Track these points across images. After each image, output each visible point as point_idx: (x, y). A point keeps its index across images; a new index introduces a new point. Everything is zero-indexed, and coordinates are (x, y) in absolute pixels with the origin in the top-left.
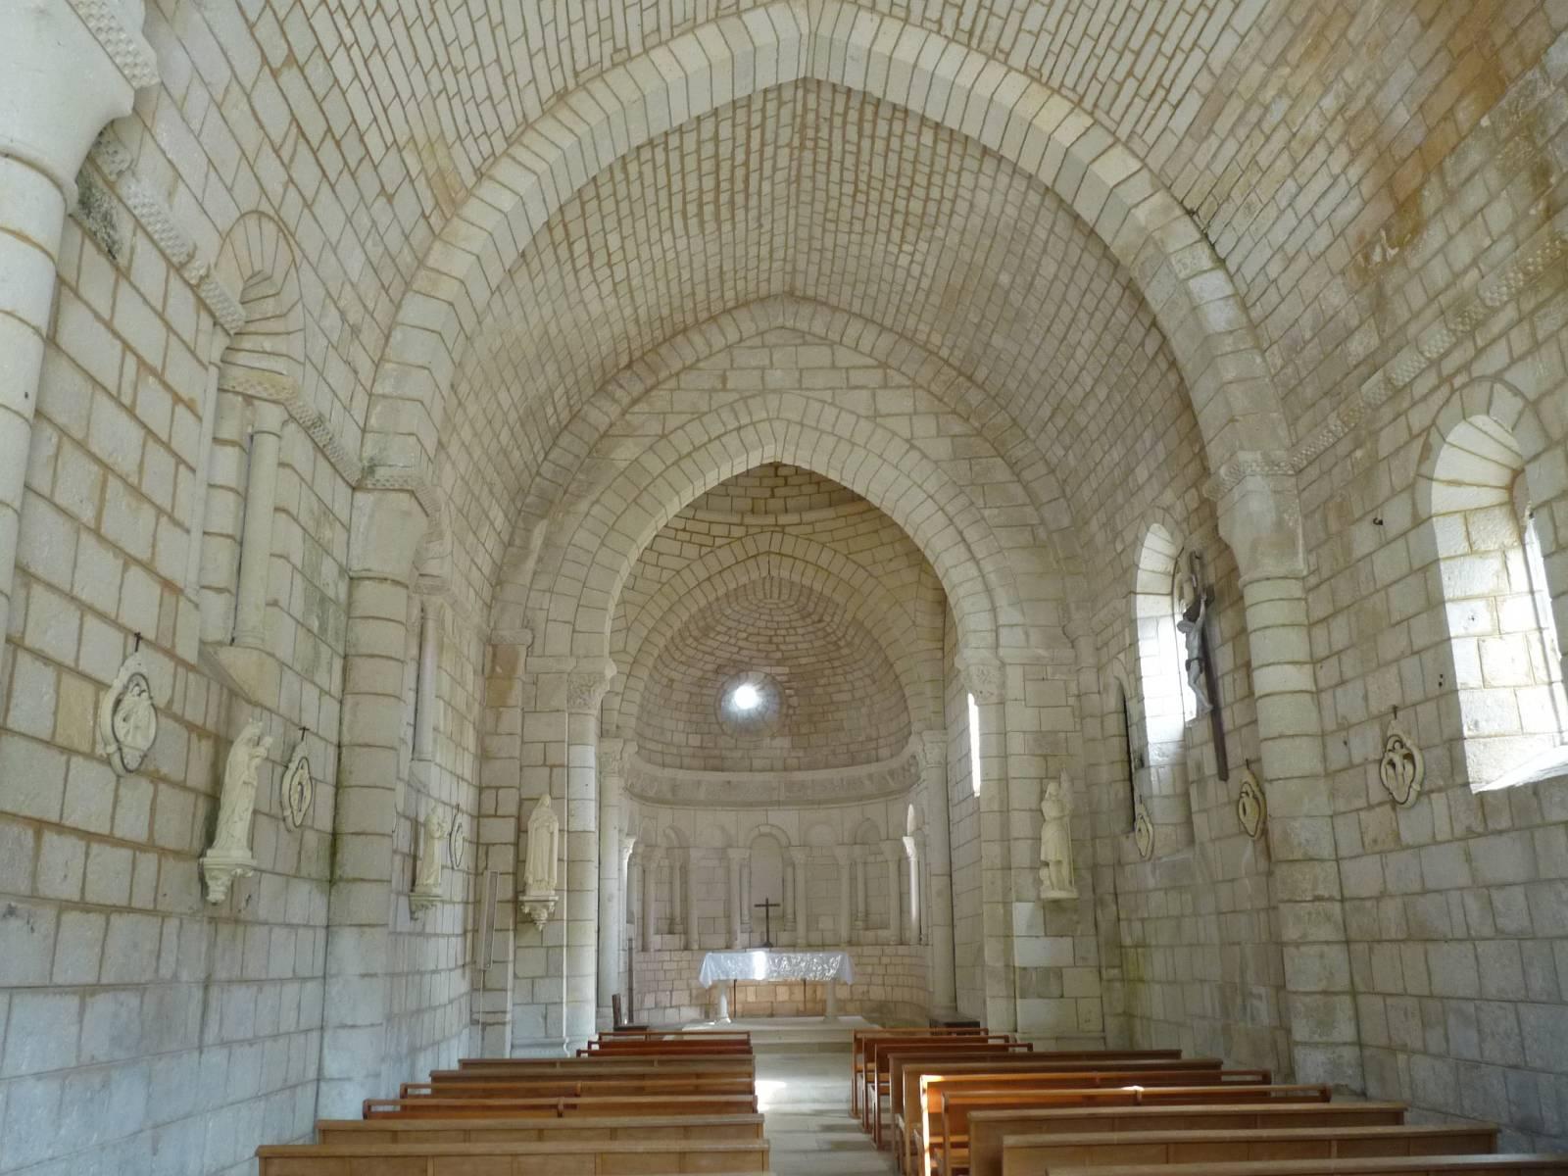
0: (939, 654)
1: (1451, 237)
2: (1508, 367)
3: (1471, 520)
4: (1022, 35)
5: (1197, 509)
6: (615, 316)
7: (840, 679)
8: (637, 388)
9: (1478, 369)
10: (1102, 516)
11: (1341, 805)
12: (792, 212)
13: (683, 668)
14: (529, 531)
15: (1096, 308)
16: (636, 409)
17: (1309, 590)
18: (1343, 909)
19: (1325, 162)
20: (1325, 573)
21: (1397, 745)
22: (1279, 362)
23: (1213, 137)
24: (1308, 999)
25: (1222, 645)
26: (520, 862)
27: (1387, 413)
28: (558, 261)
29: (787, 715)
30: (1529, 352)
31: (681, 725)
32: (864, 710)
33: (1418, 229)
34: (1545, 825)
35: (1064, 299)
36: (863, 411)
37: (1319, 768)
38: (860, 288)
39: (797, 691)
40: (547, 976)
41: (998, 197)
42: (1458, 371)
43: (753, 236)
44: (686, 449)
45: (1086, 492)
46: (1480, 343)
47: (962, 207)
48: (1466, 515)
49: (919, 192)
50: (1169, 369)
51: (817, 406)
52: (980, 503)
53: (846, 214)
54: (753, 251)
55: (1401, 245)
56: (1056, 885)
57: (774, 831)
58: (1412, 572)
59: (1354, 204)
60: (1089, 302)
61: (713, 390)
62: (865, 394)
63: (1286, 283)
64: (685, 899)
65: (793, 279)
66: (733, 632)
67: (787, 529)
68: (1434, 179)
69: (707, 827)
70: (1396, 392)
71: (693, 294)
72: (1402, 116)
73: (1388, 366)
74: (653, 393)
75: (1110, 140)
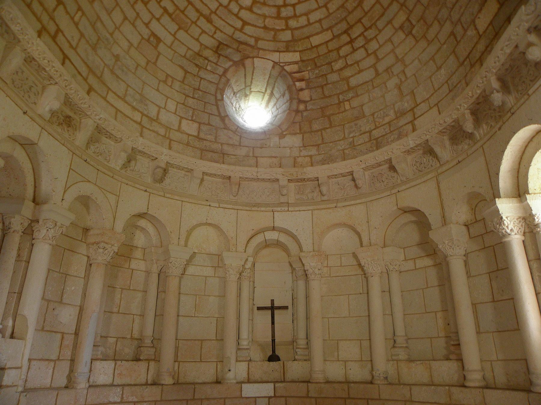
4: (283, 399)
29: (297, 111)
31: (171, 106)
32: (392, 83)
57: (283, 238)
64: (159, 315)
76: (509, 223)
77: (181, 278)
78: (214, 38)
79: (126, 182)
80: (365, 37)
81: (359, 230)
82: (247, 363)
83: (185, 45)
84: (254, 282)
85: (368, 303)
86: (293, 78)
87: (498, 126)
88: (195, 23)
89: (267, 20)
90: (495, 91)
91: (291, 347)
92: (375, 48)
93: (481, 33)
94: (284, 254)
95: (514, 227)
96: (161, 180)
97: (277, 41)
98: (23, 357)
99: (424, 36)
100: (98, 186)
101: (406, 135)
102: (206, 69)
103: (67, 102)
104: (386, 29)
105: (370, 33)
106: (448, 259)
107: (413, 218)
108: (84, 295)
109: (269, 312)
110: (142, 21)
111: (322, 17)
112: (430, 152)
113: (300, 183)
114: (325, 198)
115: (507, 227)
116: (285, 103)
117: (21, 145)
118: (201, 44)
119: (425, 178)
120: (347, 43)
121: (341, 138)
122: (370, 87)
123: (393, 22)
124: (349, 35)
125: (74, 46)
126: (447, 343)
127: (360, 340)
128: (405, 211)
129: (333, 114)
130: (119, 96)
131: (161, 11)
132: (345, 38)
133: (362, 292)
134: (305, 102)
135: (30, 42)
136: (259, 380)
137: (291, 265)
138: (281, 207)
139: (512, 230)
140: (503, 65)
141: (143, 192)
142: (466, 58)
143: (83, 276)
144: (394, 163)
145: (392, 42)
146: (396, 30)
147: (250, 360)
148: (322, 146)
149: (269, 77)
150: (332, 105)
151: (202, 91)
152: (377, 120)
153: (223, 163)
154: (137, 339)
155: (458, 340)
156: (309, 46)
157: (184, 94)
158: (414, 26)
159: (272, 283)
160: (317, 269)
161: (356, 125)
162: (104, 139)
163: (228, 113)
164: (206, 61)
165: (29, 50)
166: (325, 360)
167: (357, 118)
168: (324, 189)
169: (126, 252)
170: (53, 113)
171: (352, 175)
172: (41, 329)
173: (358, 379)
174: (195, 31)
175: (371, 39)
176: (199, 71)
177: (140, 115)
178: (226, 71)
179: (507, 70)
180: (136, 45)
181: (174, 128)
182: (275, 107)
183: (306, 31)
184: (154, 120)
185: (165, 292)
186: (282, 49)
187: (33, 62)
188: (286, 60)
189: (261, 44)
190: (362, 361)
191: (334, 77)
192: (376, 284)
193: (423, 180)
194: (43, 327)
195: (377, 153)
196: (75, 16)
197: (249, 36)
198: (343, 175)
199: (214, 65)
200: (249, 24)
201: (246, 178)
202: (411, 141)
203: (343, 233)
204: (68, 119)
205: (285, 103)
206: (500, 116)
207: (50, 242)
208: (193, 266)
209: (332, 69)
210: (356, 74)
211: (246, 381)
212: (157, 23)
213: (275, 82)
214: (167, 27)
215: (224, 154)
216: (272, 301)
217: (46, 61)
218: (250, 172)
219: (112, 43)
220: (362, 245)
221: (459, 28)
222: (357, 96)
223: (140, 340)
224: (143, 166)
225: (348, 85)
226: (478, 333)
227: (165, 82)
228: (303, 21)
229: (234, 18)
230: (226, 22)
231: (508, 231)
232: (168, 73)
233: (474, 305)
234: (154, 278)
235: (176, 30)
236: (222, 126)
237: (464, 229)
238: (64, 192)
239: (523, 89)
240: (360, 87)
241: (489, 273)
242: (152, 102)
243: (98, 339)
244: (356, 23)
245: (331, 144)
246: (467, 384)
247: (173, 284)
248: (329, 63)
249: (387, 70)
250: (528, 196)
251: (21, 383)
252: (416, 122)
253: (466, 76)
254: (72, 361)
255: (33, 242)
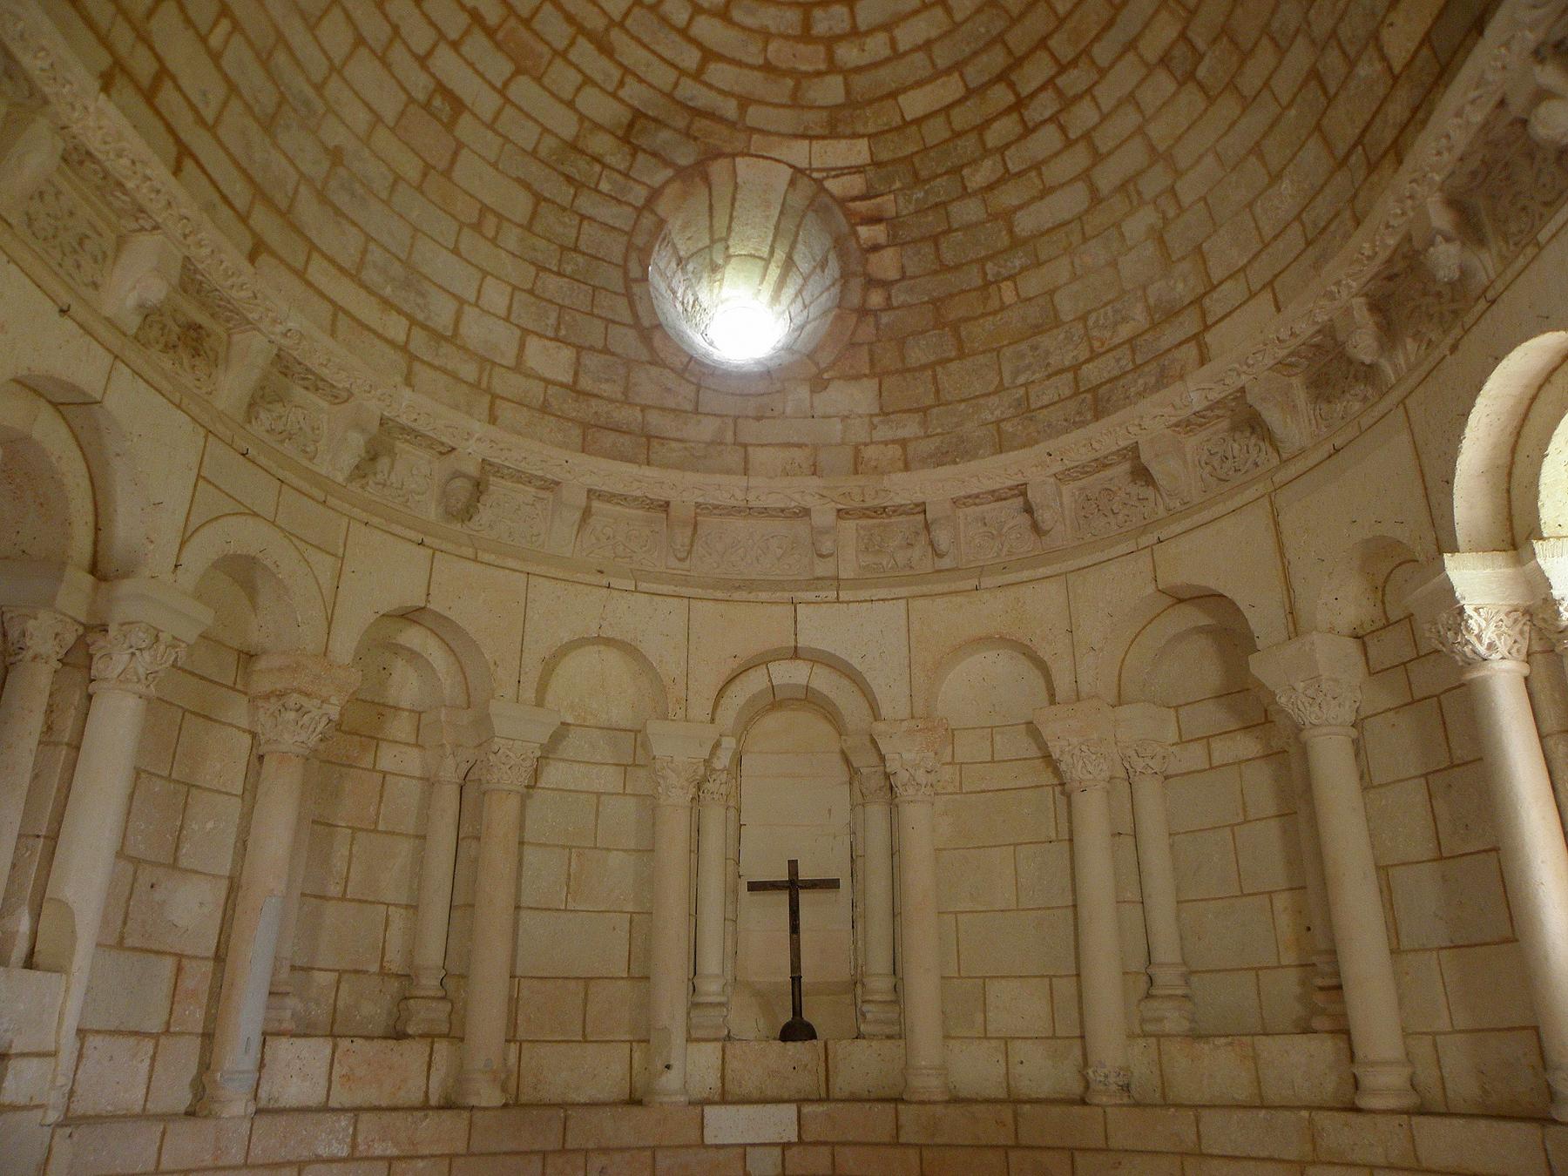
4: (825, 1150)
29: (863, 312)
31: (496, 297)
32: (1139, 224)
57: (823, 681)
64: (462, 907)
76: (1484, 624)
77: (524, 799)
78: (621, 101)
79: (365, 516)
80: (1060, 93)
81: (1045, 653)
82: (719, 1045)
83: (536, 121)
84: (739, 811)
85: (1073, 869)
86: (848, 214)
87: (1449, 341)
88: (563, 54)
89: (773, 46)
90: (1439, 238)
91: (848, 998)
92: (1090, 124)
93: (1397, 70)
94: (826, 727)
95: (1499, 636)
96: (467, 513)
97: (803, 107)
98: (60, 1024)
99: (1231, 85)
100: (282, 530)
101: (1182, 377)
102: (597, 190)
103: (190, 281)
104: (1118, 67)
105: (1074, 81)
106: (1305, 735)
107: (1204, 620)
108: (242, 847)
109: (784, 897)
110: (410, 50)
111: (934, 33)
112: (1252, 424)
113: (871, 522)
114: (946, 563)
115: (1479, 637)
116: (828, 289)
117: (56, 405)
118: (582, 118)
119: (1239, 500)
120: (1008, 110)
121: (992, 388)
122: (1076, 238)
123: (1142, 45)
124: (1012, 86)
125: (210, 120)
126: (1303, 983)
127: (1050, 977)
128: (1180, 598)
129: (966, 320)
130: (341, 269)
131: (464, 19)
132: (1001, 96)
133: (1053, 836)
134: (885, 284)
135: (78, 105)
136: (756, 1095)
137: (847, 761)
138: (817, 589)
139: (1491, 646)
140: (1461, 159)
141: (415, 548)
142: (1355, 146)
143: (240, 792)
144: (1145, 457)
145: (1138, 105)
146: (1150, 69)
147: (729, 1037)
148: (935, 410)
149: (781, 213)
150: (963, 291)
151: (584, 254)
152: (1095, 333)
153: (648, 464)
154: (398, 976)
155: (1337, 974)
156: (897, 121)
157: (533, 263)
158: (1202, 57)
159: (794, 814)
160: (922, 770)
161: (1034, 348)
162: (298, 392)
163: (662, 318)
164: (597, 168)
165: (75, 129)
166: (947, 1037)
167: (1038, 330)
168: (942, 537)
169: (364, 722)
170: (148, 314)
171: (1024, 494)
172: (119, 941)
173: (1044, 1090)
174: (566, 80)
175: (1078, 98)
176: (575, 195)
177: (405, 322)
178: (655, 194)
179: (1474, 174)
180: (390, 118)
181: (504, 362)
182: (799, 300)
183: (887, 77)
184: (446, 339)
185: (478, 839)
186: (818, 131)
187: (87, 163)
188: (831, 163)
189: (755, 116)
190: (1054, 1037)
191: (970, 211)
193: (1231, 505)
194: (122, 938)
195: (1093, 429)
196: (211, 31)
197: (721, 92)
198: (997, 496)
199: (619, 178)
200: (721, 58)
201: (716, 507)
202: (1195, 392)
203: (997, 665)
204: (193, 334)
205: (828, 289)
206: (1454, 312)
207: (141, 688)
208: (561, 765)
209: (965, 188)
210: (1033, 200)
211: (717, 1098)
212: (453, 55)
213: (799, 226)
214: (480, 67)
215: (649, 437)
216: (793, 865)
217: (125, 161)
218: (727, 488)
219: (321, 111)
220: (1052, 700)
221: (1333, 58)
222: (1039, 264)
223: (408, 977)
224: (413, 470)
225: (1011, 231)
226: (1395, 951)
227: (477, 227)
228: (877, 46)
229: (678, 39)
230: (654, 53)
231: (1482, 649)
232: (487, 201)
233: (1382, 870)
234: (447, 799)
235: (508, 74)
236: (645, 355)
237: (1352, 647)
238: (183, 544)
239: (1521, 232)
240: (1046, 238)
241: (1425, 775)
242: (440, 287)
243: (284, 974)
244: (1032, 51)
245: (963, 406)
246: (1365, 1102)
247: (502, 814)
248: (956, 171)
249: (1122, 187)
250: (1538, 546)
251: (55, 1098)
252: (1209, 337)
253: (1355, 196)
254: (208, 1036)
255: (90, 690)
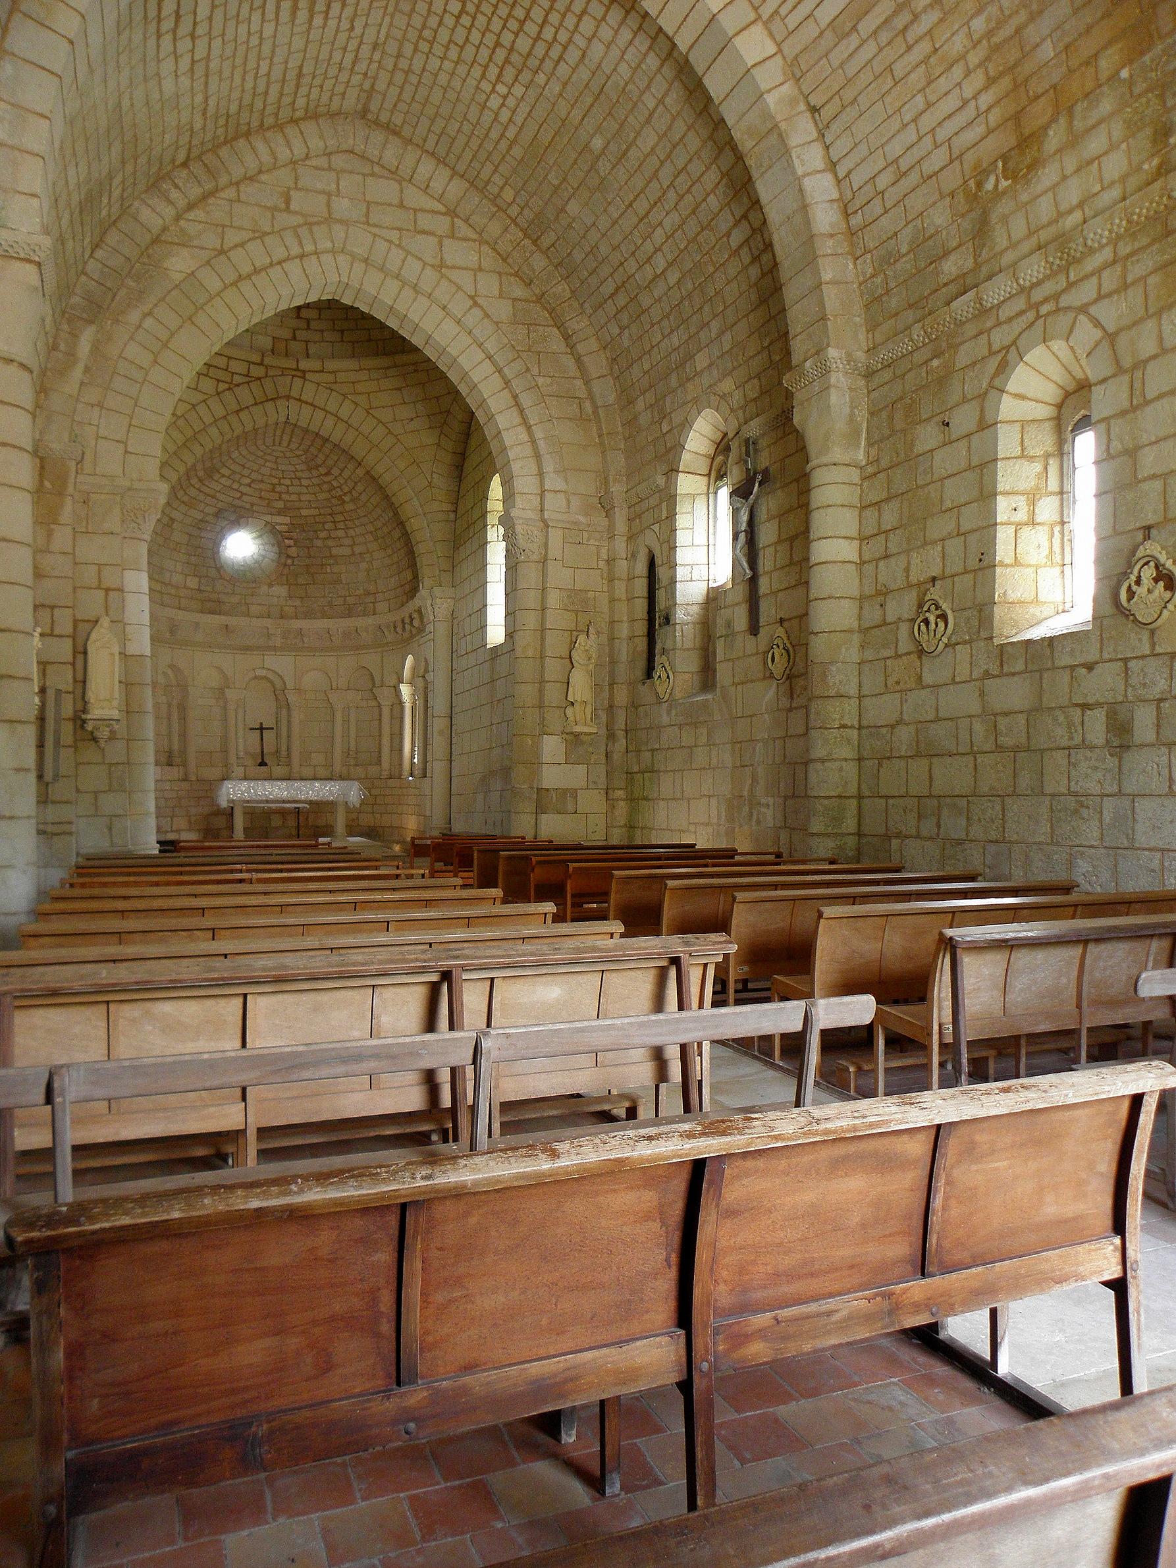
0: (452, 516)
1: (1064, 178)
2: (1095, 301)
3: (1027, 428)
5: (755, 400)
6: (185, 102)
7: (341, 533)
8: (195, 192)
9: (1065, 301)
10: (650, 397)
11: (869, 655)
12: (387, 19)
13: (183, 508)
14: (74, 336)
15: (688, 191)
16: (191, 215)
17: (863, 479)
18: (859, 735)
19: (959, 84)
20: (884, 463)
21: (933, 607)
22: (870, 271)
23: (854, 36)
24: (826, 802)
25: (768, 521)
26: (82, 682)
27: (970, 330)
28: (146, 17)
30: (1117, 291)
31: (179, 567)
33: (1034, 166)
34: (1055, 668)
35: (655, 175)
36: (430, 261)
37: (855, 625)
38: (440, 123)
39: (296, 541)
40: (110, 791)
41: (615, 52)
42: (1046, 300)
43: (343, 36)
44: (246, 269)
45: (636, 371)
46: (1072, 277)
47: (573, 55)
48: (1024, 424)
49: (531, 28)
50: (752, 262)
51: (385, 245)
52: (535, 371)
53: (443, 35)
54: (337, 56)
55: (1015, 178)
56: (583, 722)
57: (270, 676)
58: (970, 468)
59: (979, 130)
60: (683, 182)
61: (275, 209)
62: (433, 241)
63: (891, 197)
64: (183, 735)
65: (369, 98)
66: (237, 477)
67: (308, 376)
68: (1062, 121)
69: (205, 669)
70: (983, 312)
71: (266, 93)
72: (1047, 51)
73: (981, 288)
74: (211, 201)
75: (753, 16)
159: (261, 710)
167: (335, 582)
191: (319, 543)
192: (339, 715)
